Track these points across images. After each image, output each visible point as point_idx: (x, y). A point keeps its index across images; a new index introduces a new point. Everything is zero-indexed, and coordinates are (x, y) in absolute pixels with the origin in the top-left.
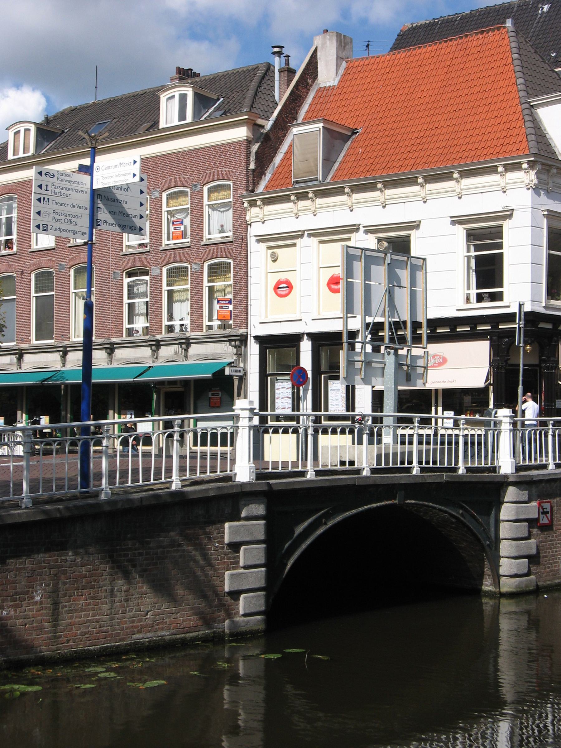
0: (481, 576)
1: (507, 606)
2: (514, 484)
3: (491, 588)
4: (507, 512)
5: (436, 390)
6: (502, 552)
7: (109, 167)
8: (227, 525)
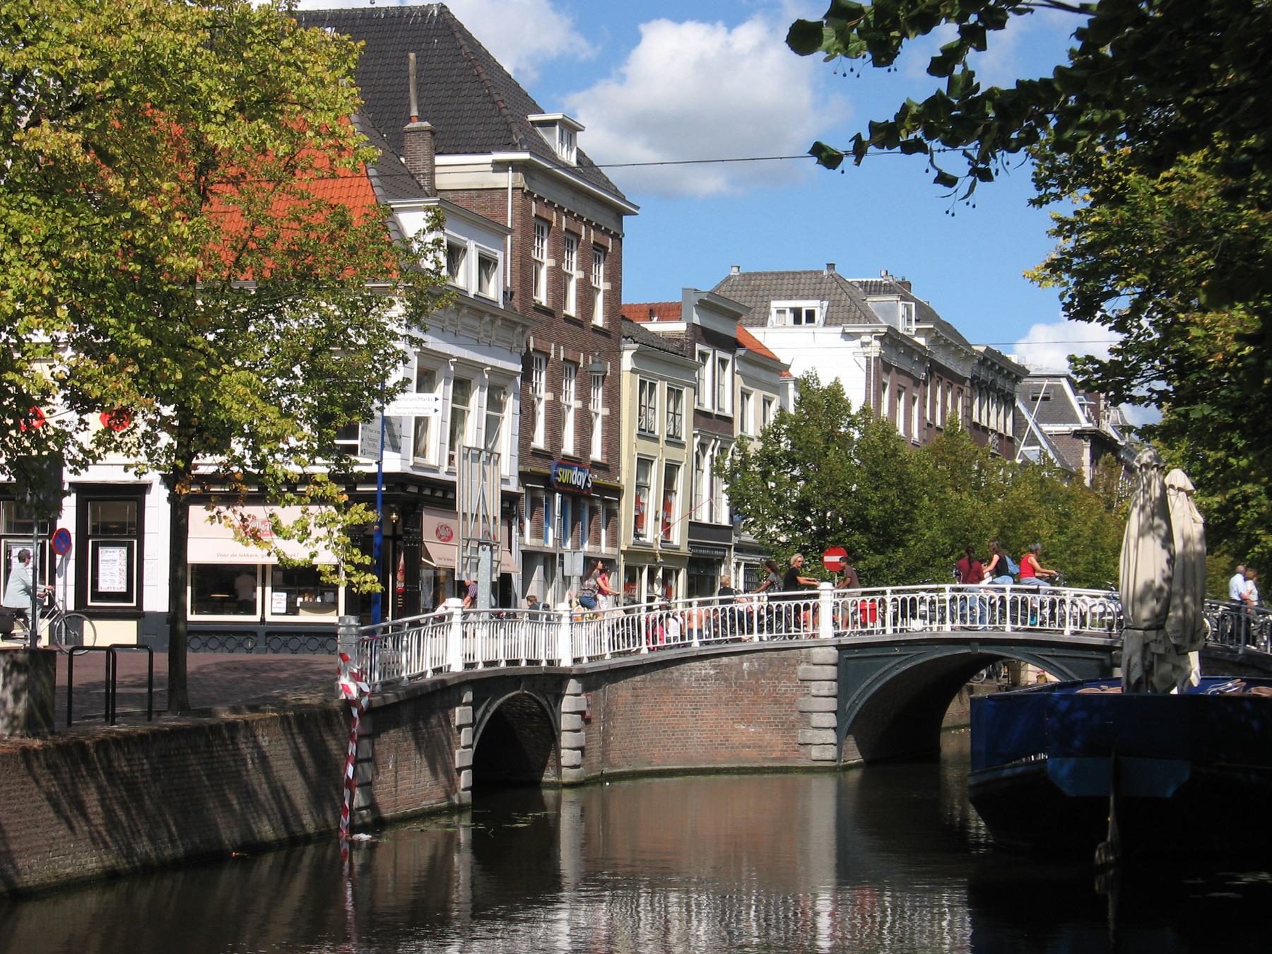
0: (543, 767)
1: (567, 795)
2: (574, 676)
3: (553, 779)
4: (567, 704)
5: (264, 566)
6: (563, 744)
7: (669, 490)
8: (457, 709)
